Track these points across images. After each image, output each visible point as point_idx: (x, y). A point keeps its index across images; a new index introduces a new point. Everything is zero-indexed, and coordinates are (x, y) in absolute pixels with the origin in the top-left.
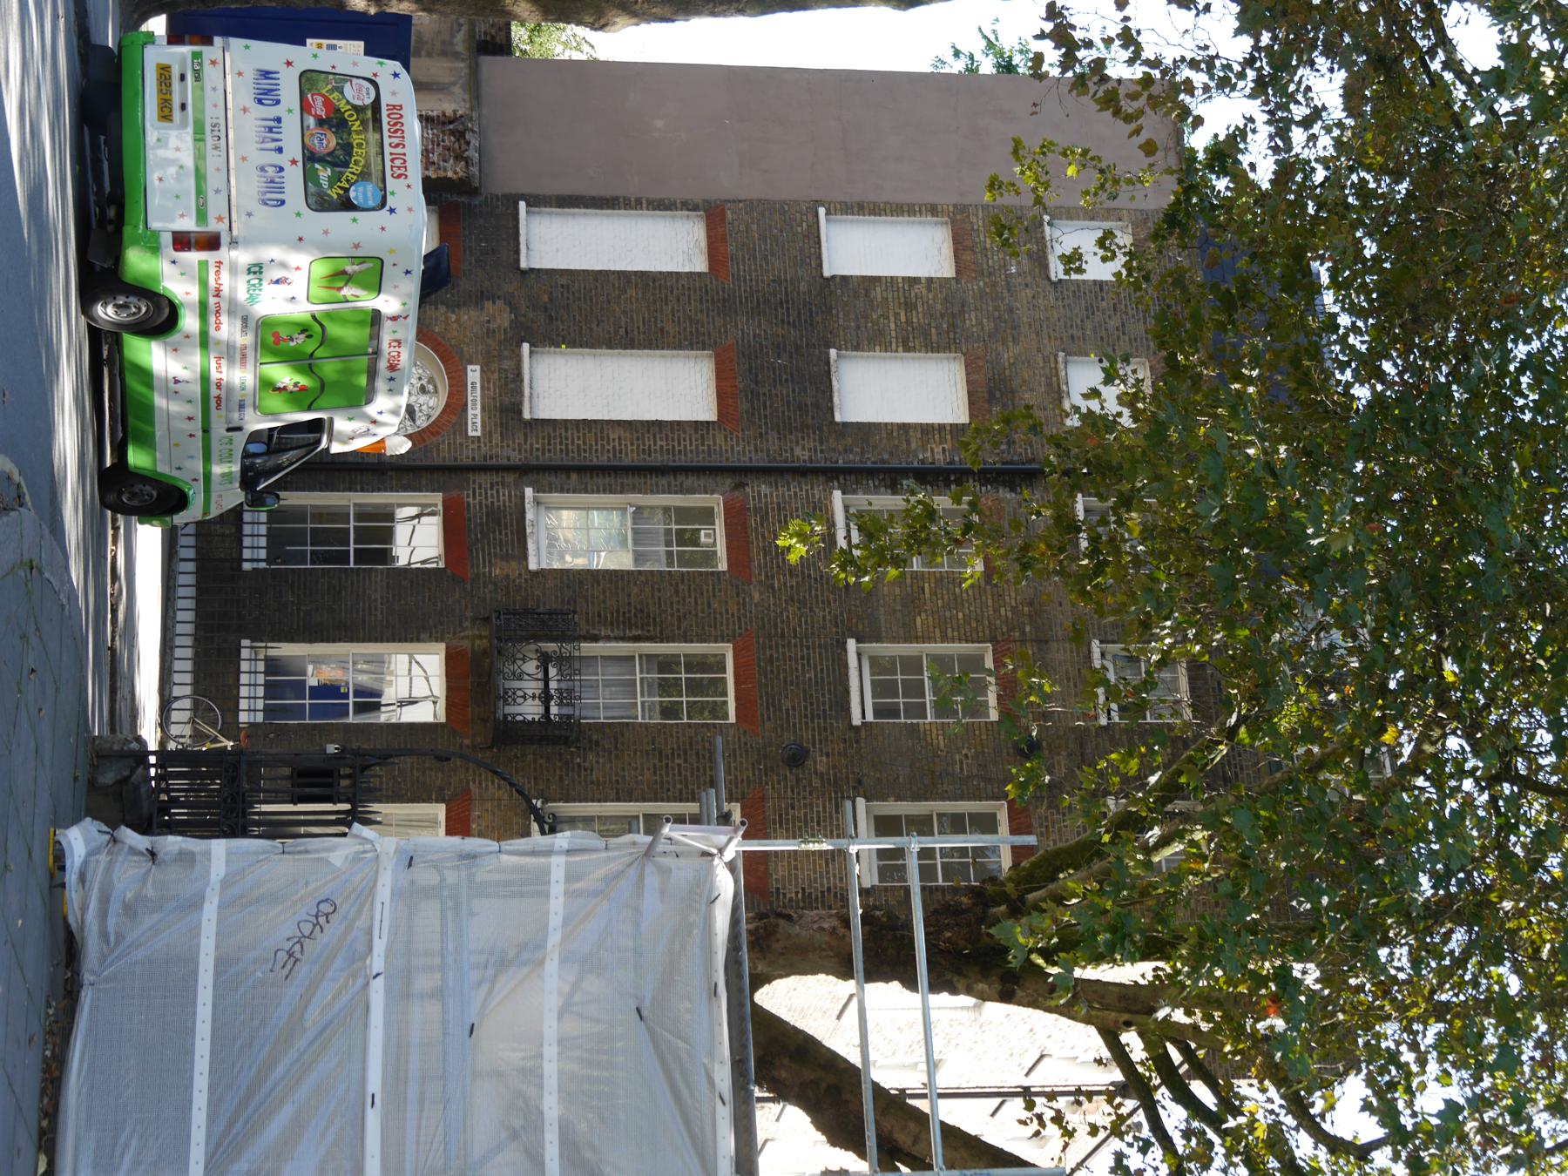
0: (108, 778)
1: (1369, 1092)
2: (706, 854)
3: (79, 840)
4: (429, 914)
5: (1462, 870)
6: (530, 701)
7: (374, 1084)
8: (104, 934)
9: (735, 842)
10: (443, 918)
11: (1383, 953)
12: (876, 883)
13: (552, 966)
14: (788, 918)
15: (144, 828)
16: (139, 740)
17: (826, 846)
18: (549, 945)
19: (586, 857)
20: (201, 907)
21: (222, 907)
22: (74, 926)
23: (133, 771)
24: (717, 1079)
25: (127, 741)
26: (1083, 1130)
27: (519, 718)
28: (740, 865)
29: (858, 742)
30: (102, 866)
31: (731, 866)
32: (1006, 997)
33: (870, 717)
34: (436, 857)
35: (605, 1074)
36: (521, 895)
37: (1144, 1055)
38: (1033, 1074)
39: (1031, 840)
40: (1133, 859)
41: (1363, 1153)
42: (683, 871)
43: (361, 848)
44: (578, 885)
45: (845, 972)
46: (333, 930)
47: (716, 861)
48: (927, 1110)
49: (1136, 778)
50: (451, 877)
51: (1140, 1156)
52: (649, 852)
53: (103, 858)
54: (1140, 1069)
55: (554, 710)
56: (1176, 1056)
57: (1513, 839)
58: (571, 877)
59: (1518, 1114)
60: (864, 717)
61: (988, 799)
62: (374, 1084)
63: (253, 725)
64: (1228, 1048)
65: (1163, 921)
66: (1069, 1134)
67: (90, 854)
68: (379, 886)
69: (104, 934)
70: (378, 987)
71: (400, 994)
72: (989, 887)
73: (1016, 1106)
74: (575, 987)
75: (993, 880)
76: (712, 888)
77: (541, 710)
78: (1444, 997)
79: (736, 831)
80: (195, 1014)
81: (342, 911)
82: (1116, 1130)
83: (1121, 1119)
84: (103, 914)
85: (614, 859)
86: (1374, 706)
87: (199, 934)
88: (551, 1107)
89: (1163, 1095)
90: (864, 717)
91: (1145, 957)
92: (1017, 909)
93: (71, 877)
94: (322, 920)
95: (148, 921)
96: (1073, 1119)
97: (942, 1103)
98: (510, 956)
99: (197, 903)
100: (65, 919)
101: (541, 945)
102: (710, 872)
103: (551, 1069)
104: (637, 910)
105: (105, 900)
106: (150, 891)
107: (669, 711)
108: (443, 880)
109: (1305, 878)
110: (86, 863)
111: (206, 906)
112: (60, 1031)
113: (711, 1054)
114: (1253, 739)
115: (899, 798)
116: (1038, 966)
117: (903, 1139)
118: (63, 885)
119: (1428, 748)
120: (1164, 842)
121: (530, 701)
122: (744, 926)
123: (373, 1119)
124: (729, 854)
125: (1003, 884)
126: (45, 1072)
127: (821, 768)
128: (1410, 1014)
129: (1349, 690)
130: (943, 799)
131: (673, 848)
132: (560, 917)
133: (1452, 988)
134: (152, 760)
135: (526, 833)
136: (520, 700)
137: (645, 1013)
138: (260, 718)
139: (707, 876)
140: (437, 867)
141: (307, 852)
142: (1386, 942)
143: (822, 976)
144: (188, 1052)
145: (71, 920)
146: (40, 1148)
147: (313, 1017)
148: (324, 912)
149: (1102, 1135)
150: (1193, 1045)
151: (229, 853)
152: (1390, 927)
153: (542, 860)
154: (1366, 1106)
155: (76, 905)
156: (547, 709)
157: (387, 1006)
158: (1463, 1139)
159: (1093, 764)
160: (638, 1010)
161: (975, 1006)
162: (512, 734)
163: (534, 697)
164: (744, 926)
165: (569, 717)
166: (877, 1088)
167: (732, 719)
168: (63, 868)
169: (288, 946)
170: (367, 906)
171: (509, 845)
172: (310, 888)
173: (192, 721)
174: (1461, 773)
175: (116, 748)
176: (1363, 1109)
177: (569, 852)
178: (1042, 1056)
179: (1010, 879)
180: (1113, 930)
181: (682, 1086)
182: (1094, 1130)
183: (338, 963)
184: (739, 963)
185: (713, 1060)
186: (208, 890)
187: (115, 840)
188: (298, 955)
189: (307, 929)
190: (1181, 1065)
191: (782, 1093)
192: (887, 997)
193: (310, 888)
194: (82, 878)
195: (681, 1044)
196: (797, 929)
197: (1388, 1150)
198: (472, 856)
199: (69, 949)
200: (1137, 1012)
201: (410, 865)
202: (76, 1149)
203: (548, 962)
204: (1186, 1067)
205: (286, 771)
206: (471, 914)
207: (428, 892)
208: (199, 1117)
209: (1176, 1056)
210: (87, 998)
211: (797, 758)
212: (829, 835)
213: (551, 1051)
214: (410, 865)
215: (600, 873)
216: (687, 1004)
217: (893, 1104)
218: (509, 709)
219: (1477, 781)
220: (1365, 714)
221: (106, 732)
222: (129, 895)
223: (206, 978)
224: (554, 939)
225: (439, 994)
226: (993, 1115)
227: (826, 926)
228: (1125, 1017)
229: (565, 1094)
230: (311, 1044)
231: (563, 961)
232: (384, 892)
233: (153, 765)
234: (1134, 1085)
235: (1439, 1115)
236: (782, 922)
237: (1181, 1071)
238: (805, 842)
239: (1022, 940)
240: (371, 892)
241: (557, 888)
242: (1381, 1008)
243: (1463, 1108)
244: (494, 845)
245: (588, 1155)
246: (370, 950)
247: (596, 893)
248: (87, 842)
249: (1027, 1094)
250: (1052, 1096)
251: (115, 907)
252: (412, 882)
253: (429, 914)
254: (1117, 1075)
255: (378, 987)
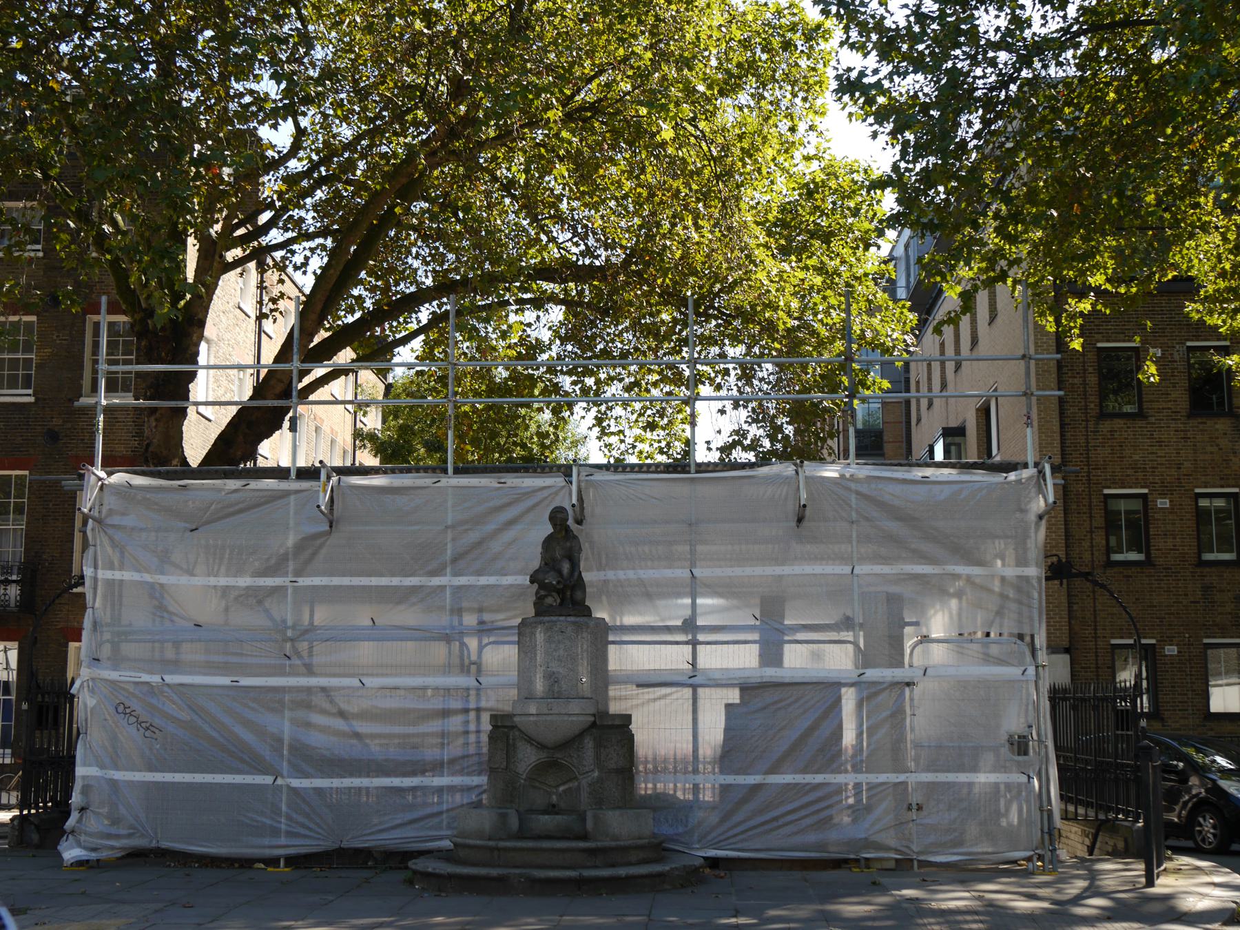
0: (35, 837)
1: (267, 124)
2: (102, 488)
3: (71, 852)
4: (128, 649)
5: (139, 53)
6: (8, 592)
7: (225, 681)
8: (129, 836)
9: (96, 472)
10: (131, 641)
11: (185, 104)
12: (131, 394)
13: (163, 579)
14: (148, 445)
15: (67, 815)
16: (12, 820)
17: (101, 418)
18: (151, 580)
19: (99, 558)
20: (116, 781)
21: (117, 768)
22: (123, 854)
23: (32, 823)
24: (234, 487)
25: (13, 827)
26: (280, 287)
27: (18, 598)
28: (109, 469)
29: (45, 399)
30: (88, 838)
31: (110, 474)
32: (202, 324)
33: (30, 391)
34: (94, 645)
35: (228, 551)
36: (120, 596)
37: (239, 249)
38: (249, 313)
39: (104, 299)
40: (120, 241)
41: (300, 133)
42: (111, 501)
43: (86, 689)
44: (116, 563)
45: (183, 413)
46: (135, 705)
47: (106, 482)
48: (266, 370)
49: (71, 235)
50: (107, 636)
51: (296, 255)
52: (99, 521)
53: (83, 838)
54: (248, 252)
55: (14, 577)
56: (241, 232)
57: (122, 20)
58: (112, 568)
59: (285, 41)
60: (29, 395)
61: (84, 326)
62: (225, 681)
63: (13, 755)
64: (234, 200)
65: (159, 228)
66: (282, 295)
67: (79, 845)
68: (109, 678)
69: (129, 836)
70: (169, 679)
71: (175, 666)
72: (136, 329)
73: (267, 325)
74: (177, 566)
75: (132, 325)
76: (122, 486)
77: (14, 585)
78: (216, 75)
79: (88, 470)
80: (179, 783)
81: (123, 699)
82: (282, 269)
83: (276, 265)
84: (118, 837)
85: (101, 541)
86: (36, 90)
87: (132, 782)
88: (244, 581)
89: (265, 240)
90: (29, 395)
91: (184, 243)
92: (150, 313)
93: (93, 856)
94: (128, 711)
95: (123, 810)
96: (275, 292)
97: (262, 362)
98: (157, 603)
99: (113, 783)
100: (118, 859)
101: (152, 586)
102: (110, 485)
103: (223, 581)
104: (133, 529)
105: (109, 836)
106: (105, 810)
107: (19, 510)
108: (108, 641)
109: (138, 143)
110: (85, 848)
111: (115, 777)
112: (184, 859)
113: (220, 490)
114: (55, 167)
115: (81, 377)
116: (185, 304)
117: (279, 388)
118: (98, 861)
119: (65, 63)
120: (114, 223)
121: (8, 592)
122: (152, 468)
123: (246, 681)
124: (102, 474)
125: (135, 321)
126: (207, 866)
127: (60, 422)
128: (223, 95)
129: (24, 104)
130: (83, 352)
131: (97, 507)
132: (134, 574)
133: (210, 70)
134: (25, 812)
135: (83, 595)
136: (7, 598)
137: (194, 527)
138: (8, 751)
139: (117, 490)
140: (100, 645)
141: (86, 720)
142: (179, 102)
143: (184, 428)
144: (202, 786)
145: (119, 855)
146: (251, 868)
147: (185, 715)
148: (123, 710)
149: (284, 277)
150: (236, 221)
151: (84, 765)
152: (171, 98)
153: (100, 583)
154: (275, 126)
155: (110, 853)
156: (14, 581)
157: (181, 673)
158: (294, 73)
159: (62, 260)
160: (192, 531)
161: (208, 342)
162: (28, 602)
163: (5, 589)
164: (152, 468)
165: (19, 569)
166: (251, 398)
167: (26, 473)
168: (88, 861)
169: (142, 731)
170: (122, 685)
171: (89, 603)
172: (108, 717)
173: (8, 791)
174: (82, 46)
175: (16, 833)
176: (276, 129)
177: (96, 567)
178: (239, 308)
179: (132, 317)
180: (163, 257)
181: (237, 508)
182: (281, 281)
183: (154, 701)
184: (168, 472)
185: (223, 490)
186: (106, 776)
187: (72, 832)
188: (148, 725)
189: (133, 720)
190: (247, 228)
191: (252, 454)
192: (200, 389)
193: (108, 717)
194: (94, 850)
195: (213, 507)
196: (155, 441)
197: (300, 118)
198: (95, 624)
199: (136, 857)
200: (215, 251)
201: (98, 660)
202: (252, 847)
203: (161, 581)
204: (248, 226)
205: (38, 733)
206: (130, 625)
207: (116, 648)
208: (238, 779)
209: (241, 232)
210: (165, 844)
211: (53, 436)
212: (95, 416)
213: (213, 581)
214: (98, 660)
215: (109, 550)
216: (190, 502)
217: (260, 390)
218: (13, 604)
219: (87, 38)
220: (40, 96)
221: (7, 841)
222: (106, 822)
223: (158, 777)
224: (147, 577)
225: (177, 644)
226: (271, 338)
227: (154, 424)
228: (217, 257)
229: (239, 572)
230: (200, 717)
231: (162, 573)
232: (113, 675)
233: (29, 811)
234: (260, 255)
235: (278, 83)
236: (151, 449)
237: (251, 229)
238: (98, 430)
239: (166, 310)
240: (113, 682)
241: (117, 575)
242: (218, 111)
243: (275, 70)
244: (89, 611)
245: (273, 561)
246: (147, 683)
247: (122, 553)
248: (72, 848)
249: (261, 317)
250: (260, 302)
251: (113, 830)
252: (109, 659)
253: (128, 649)
254: (252, 265)
255: (169, 679)
